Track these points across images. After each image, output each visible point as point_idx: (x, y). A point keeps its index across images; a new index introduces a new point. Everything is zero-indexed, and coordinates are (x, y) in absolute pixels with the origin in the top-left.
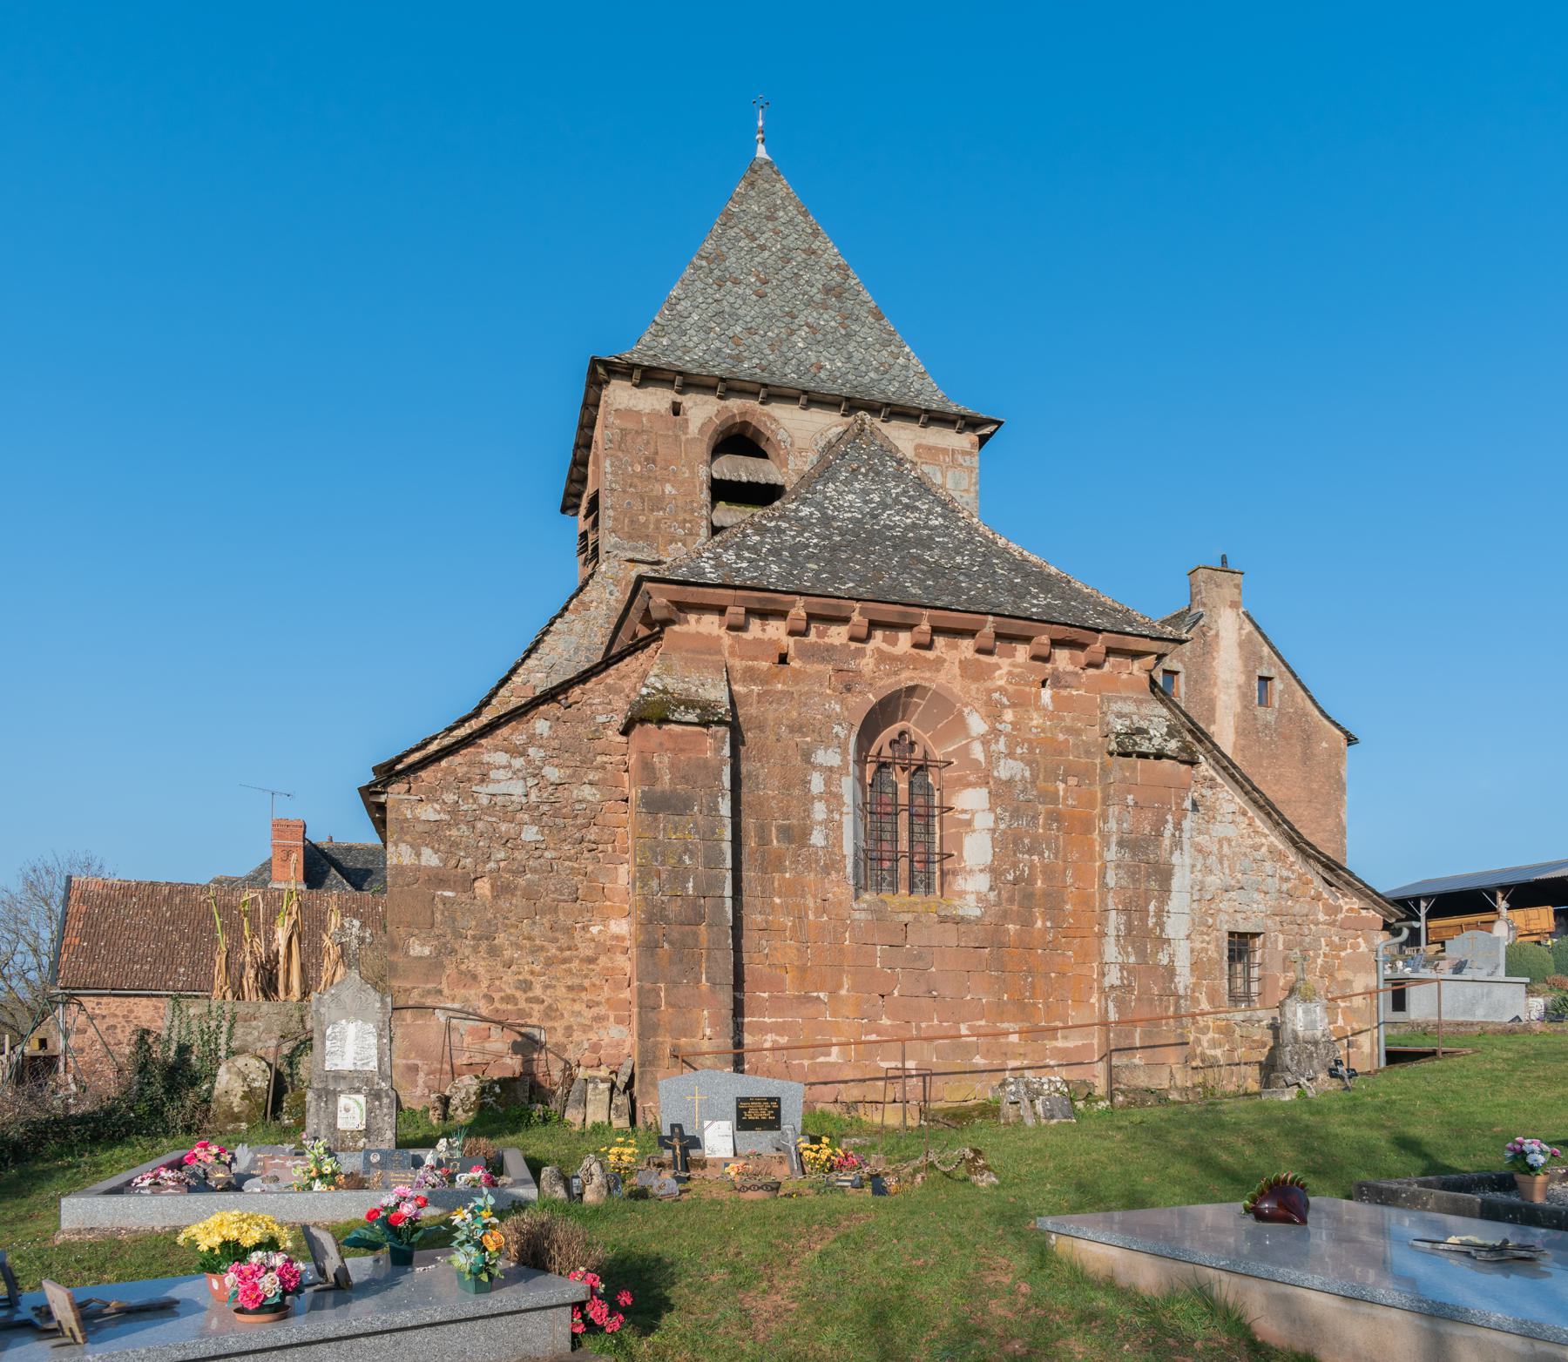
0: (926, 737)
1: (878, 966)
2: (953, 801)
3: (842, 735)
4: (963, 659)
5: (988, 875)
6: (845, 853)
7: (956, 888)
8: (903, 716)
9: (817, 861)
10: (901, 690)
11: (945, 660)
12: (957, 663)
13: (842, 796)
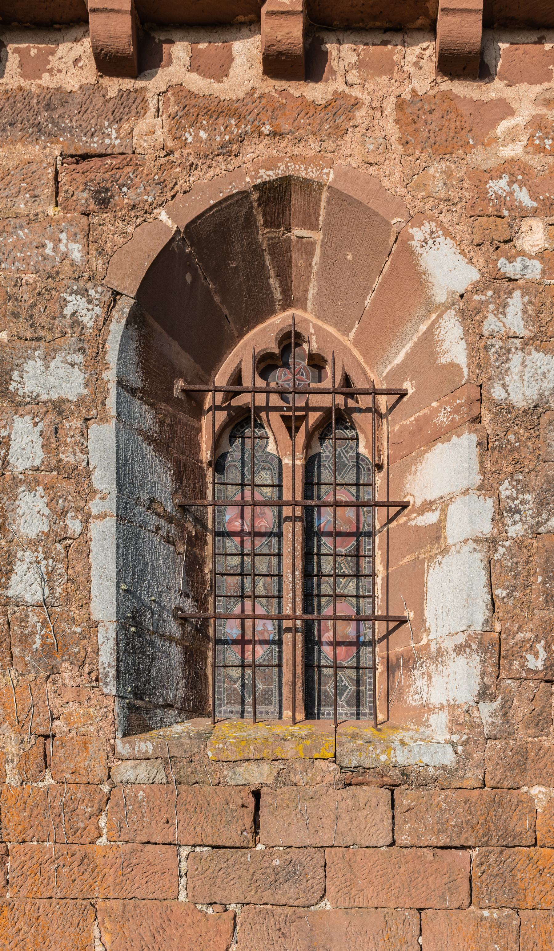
0: (348, 341)
1: (182, 897)
2: (408, 488)
3: (88, 320)
4: (407, 96)
5: (477, 659)
6: (95, 616)
7: (412, 700)
8: (286, 291)
9: (25, 639)
10: (244, 195)
11: (357, 104)
12: (390, 106)
13: (88, 474)
